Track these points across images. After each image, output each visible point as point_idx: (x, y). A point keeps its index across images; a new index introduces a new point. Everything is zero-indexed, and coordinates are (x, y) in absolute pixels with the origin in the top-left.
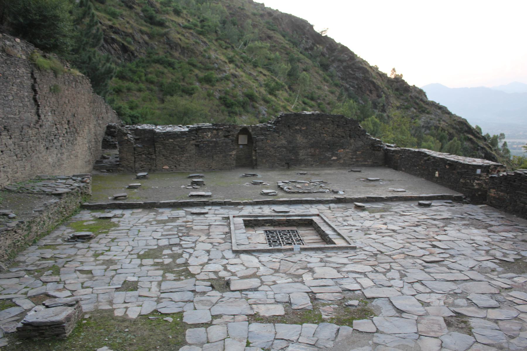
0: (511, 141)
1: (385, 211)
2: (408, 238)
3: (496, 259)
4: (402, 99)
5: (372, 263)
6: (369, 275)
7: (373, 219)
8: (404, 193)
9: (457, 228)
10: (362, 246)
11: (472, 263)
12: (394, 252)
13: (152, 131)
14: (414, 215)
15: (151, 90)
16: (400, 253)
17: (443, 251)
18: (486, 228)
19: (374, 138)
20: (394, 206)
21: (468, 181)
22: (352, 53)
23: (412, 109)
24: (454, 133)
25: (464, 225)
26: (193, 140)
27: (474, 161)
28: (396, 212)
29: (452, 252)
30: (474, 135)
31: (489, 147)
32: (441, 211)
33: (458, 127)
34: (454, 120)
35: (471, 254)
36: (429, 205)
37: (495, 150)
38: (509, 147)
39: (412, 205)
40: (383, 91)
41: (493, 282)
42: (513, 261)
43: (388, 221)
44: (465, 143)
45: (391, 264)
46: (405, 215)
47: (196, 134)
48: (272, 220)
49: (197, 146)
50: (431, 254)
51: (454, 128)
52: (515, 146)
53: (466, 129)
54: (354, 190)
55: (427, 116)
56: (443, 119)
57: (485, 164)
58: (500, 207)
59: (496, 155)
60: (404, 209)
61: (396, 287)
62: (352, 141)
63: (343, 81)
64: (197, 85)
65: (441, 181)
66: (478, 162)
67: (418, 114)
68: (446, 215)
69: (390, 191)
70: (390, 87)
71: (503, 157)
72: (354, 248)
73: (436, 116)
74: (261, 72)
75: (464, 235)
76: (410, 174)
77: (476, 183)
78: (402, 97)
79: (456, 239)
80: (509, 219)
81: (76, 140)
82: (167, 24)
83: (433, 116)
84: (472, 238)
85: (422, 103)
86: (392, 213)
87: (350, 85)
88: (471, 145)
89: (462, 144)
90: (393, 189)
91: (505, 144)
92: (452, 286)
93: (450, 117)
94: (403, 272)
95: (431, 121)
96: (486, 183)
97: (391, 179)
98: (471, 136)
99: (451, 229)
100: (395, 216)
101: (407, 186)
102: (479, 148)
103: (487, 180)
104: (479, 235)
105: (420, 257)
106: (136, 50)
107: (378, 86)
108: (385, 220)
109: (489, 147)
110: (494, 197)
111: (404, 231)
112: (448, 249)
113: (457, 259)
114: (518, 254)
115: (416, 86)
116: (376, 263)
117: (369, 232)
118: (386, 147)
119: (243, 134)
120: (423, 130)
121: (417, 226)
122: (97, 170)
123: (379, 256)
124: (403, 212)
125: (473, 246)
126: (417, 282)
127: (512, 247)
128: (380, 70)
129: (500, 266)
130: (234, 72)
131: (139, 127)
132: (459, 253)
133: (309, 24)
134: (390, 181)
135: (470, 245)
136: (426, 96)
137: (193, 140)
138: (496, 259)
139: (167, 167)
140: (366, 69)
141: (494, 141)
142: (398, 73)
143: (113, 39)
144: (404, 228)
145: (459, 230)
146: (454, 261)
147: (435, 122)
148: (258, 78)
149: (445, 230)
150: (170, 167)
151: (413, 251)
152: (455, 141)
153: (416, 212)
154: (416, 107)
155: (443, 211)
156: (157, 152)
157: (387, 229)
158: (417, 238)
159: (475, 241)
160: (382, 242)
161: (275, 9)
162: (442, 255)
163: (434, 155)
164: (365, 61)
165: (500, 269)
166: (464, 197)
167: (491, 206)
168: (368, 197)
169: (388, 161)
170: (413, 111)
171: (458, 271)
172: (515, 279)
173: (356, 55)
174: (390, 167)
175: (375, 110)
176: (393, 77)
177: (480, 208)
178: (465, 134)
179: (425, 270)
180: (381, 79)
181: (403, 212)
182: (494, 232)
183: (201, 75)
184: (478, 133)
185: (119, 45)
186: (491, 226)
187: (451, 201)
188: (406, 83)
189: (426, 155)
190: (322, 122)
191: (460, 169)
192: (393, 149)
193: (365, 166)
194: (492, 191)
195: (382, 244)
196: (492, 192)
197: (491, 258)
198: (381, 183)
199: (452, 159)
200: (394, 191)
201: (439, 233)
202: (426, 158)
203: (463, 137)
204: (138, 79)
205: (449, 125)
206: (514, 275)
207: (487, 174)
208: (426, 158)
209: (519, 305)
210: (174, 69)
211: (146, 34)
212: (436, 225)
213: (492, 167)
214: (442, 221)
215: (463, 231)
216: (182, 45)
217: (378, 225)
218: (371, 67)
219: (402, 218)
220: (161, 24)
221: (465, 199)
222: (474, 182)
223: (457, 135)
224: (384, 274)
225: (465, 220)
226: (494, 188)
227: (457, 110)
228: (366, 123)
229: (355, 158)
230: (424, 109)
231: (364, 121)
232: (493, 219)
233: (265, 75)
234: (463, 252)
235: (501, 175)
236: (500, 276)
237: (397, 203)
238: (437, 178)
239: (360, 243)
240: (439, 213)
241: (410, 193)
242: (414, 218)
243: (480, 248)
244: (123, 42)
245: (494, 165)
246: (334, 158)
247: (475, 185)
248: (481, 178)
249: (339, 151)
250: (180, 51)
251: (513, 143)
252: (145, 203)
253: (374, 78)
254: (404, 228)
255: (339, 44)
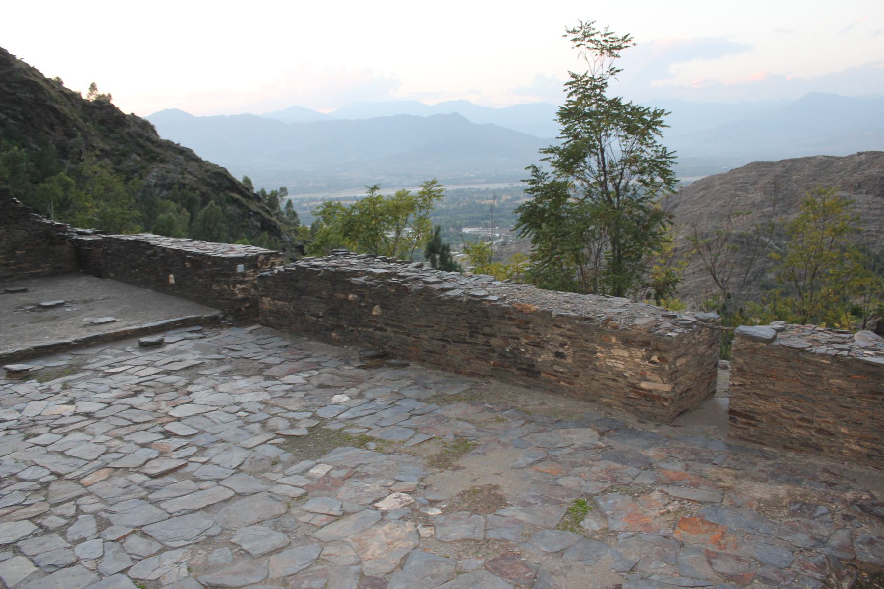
0: (299, 196)
1: (74, 372)
2: (118, 427)
3: (279, 435)
4: (114, 139)
5: (34, 511)
6: (25, 546)
7: (45, 395)
8: (112, 326)
9: (211, 383)
10: (14, 471)
11: (236, 457)
12: (86, 468)
14: (131, 371)
16: (99, 469)
17: (184, 442)
18: (260, 372)
19: (48, 222)
20: (94, 356)
21: (226, 287)
23: (134, 156)
24: (210, 192)
25: (224, 373)
27: (232, 250)
28: (96, 370)
29: (202, 440)
30: (241, 193)
31: (267, 211)
32: (181, 352)
33: (214, 182)
34: (207, 171)
35: (237, 435)
36: (159, 344)
37: (276, 214)
38: (296, 208)
39: (128, 348)
40: (75, 125)
41: (276, 489)
42: (305, 432)
43: (78, 395)
44: (229, 208)
45: (79, 501)
46: (113, 373)
50: (162, 454)
51: (208, 184)
52: (305, 205)
53: (228, 184)
54: (10, 335)
55: (161, 166)
56: (189, 170)
57: (250, 254)
58: (282, 326)
59: (277, 221)
60: (111, 359)
61: (87, 560)
65: (180, 292)
66: (238, 250)
67: (145, 163)
68: (191, 359)
69: (85, 326)
70: (88, 117)
71: (288, 224)
73: (175, 165)
75: (223, 396)
76: (126, 282)
77: (239, 289)
78: (112, 135)
79: (209, 408)
80: (297, 346)
83: (171, 166)
84: (238, 399)
85: (149, 144)
86: (88, 373)
87: (7, 114)
88: (239, 211)
89: (223, 211)
90: (91, 319)
91: (290, 203)
92: (204, 521)
93: (200, 166)
94: (104, 515)
95: (169, 175)
96: (255, 287)
97: (88, 298)
98: (236, 196)
99: (200, 387)
100: (94, 380)
101: (118, 309)
102: (251, 213)
103: (256, 282)
104: (248, 391)
105: (138, 469)
107: (65, 115)
108: (71, 394)
109: (267, 211)
110: (270, 311)
111: (110, 411)
112: (194, 435)
113: (212, 452)
114: (314, 416)
115: (137, 114)
116: (45, 507)
117: (34, 431)
118: (76, 237)
120: (157, 190)
121: (136, 393)
123: (53, 487)
125: (239, 418)
126: (134, 532)
127: (304, 404)
128: (66, 85)
129: (287, 450)
132: (213, 439)
134: (86, 302)
135: (233, 417)
136: (155, 132)
138: (279, 435)
140: (36, 84)
141: (273, 200)
142: (102, 91)
144: (110, 404)
145: (213, 388)
146: (204, 459)
147: (174, 176)
149: (189, 393)
151: (126, 455)
152: (212, 206)
153: (133, 362)
154: (139, 151)
155: (185, 352)
157: (75, 414)
158: (136, 423)
159: (243, 406)
160: (60, 450)
162: (183, 453)
163: (164, 244)
164: (33, 69)
165: (286, 457)
166: (221, 316)
167: (266, 326)
168: (36, 348)
169: (85, 262)
170: (135, 160)
171: (213, 483)
172: (313, 471)
173: (13, 57)
174: (87, 273)
175: (65, 161)
176: (93, 98)
177: (250, 333)
178: (227, 192)
179: (150, 496)
180: (69, 103)
181: (110, 366)
182: (274, 378)
184: (247, 190)
186: (268, 366)
187: (200, 328)
188: (117, 110)
189: (149, 246)
191: (210, 267)
192: (89, 238)
193: (37, 276)
194: (266, 300)
195: (62, 453)
196: (266, 303)
197: (271, 436)
198: (68, 310)
199: (194, 250)
200: (93, 324)
201: (178, 401)
202: (149, 252)
203: (225, 198)
205: (199, 179)
206: (309, 463)
207: (255, 272)
208: (149, 252)
209: (322, 527)
212: (171, 385)
213: (261, 258)
214: (183, 373)
215: (221, 388)
217: (57, 408)
218: (47, 81)
219: (106, 381)
221: (224, 319)
222: (235, 287)
223: (214, 195)
224: (62, 531)
225: (225, 364)
226: (266, 296)
227: (209, 153)
228: (47, 186)
229: (14, 265)
230: (153, 154)
231: (44, 182)
232: (271, 352)
234: (222, 436)
235: (276, 272)
236: (287, 472)
237: (98, 350)
238: (172, 285)
239: (12, 462)
240: (179, 357)
241: (125, 323)
242: (130, 377)
243: (252, 418)
245: (265, 254)
247: (237, 292)
248: (246, 279)
251: (302, 200)
253: (57, 102)
254: (110, 404)
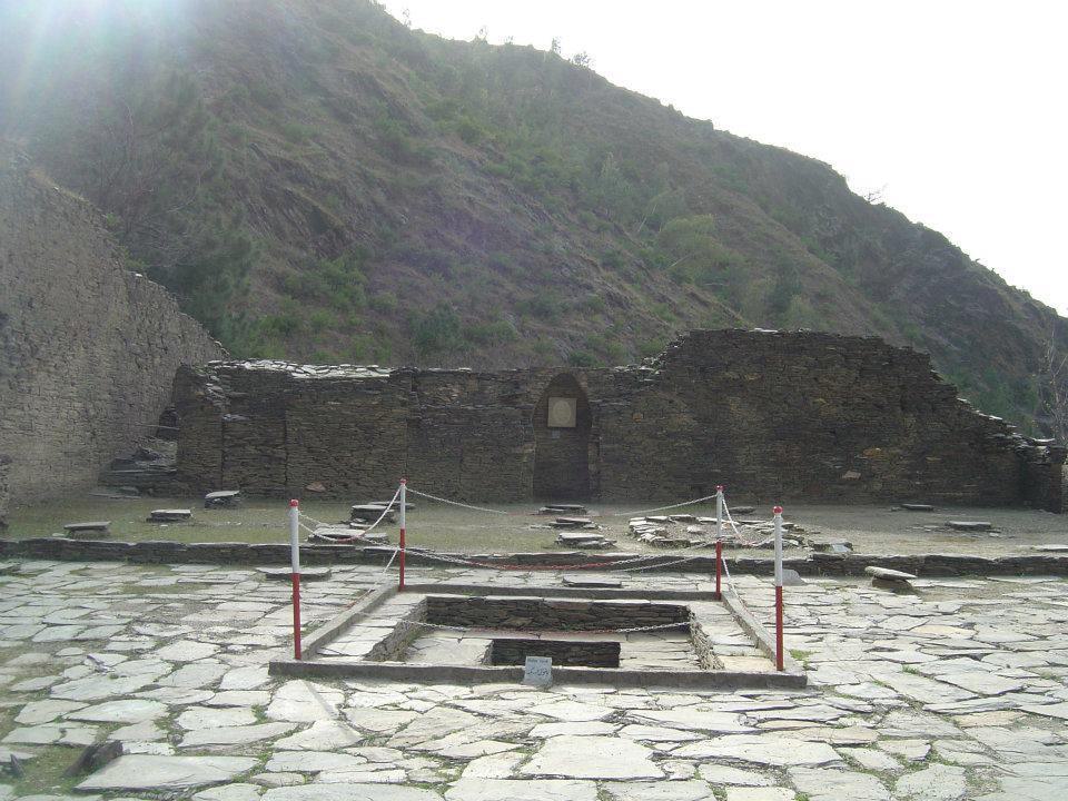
13: (284, 377)
15: (380, 332)
22: (956, 251)
26: (404, 404)
47: (414, 389)
48: (536, 603)
49: (414, 424)
62: (910, 420)
63: (930, 329)
64: (510, 321)
72: (798, 683)
74: (693, 295)
81: (31, 377)
82: (438, 162)
106: (349, 226)
119: (564, 395)
122: (110, 486)
124: (1054, 599)
130: (615, 290)
131: (248, 366)
133: (835, 173)
137: (404, 404)
139: (320, 487)
143: (288, 194)
148: (684, 310)
150: (329, 487)
156: (289, 439)
161: (743, 136)
174: (1035, 505)
183: (524, 296)
185: (304, 212)
190: (811, 359)
204: (346, 300)
210: (448, 277)
211: (381, 184)
216: (476, 216)
218: (1011, 290)
220: (423, 162)
233: (705, 304)
244: (316, 204)
246: (851, 475)
249: (868, 452)
250: (469, 232)
252: (140, 546)
255: (920, 226)
